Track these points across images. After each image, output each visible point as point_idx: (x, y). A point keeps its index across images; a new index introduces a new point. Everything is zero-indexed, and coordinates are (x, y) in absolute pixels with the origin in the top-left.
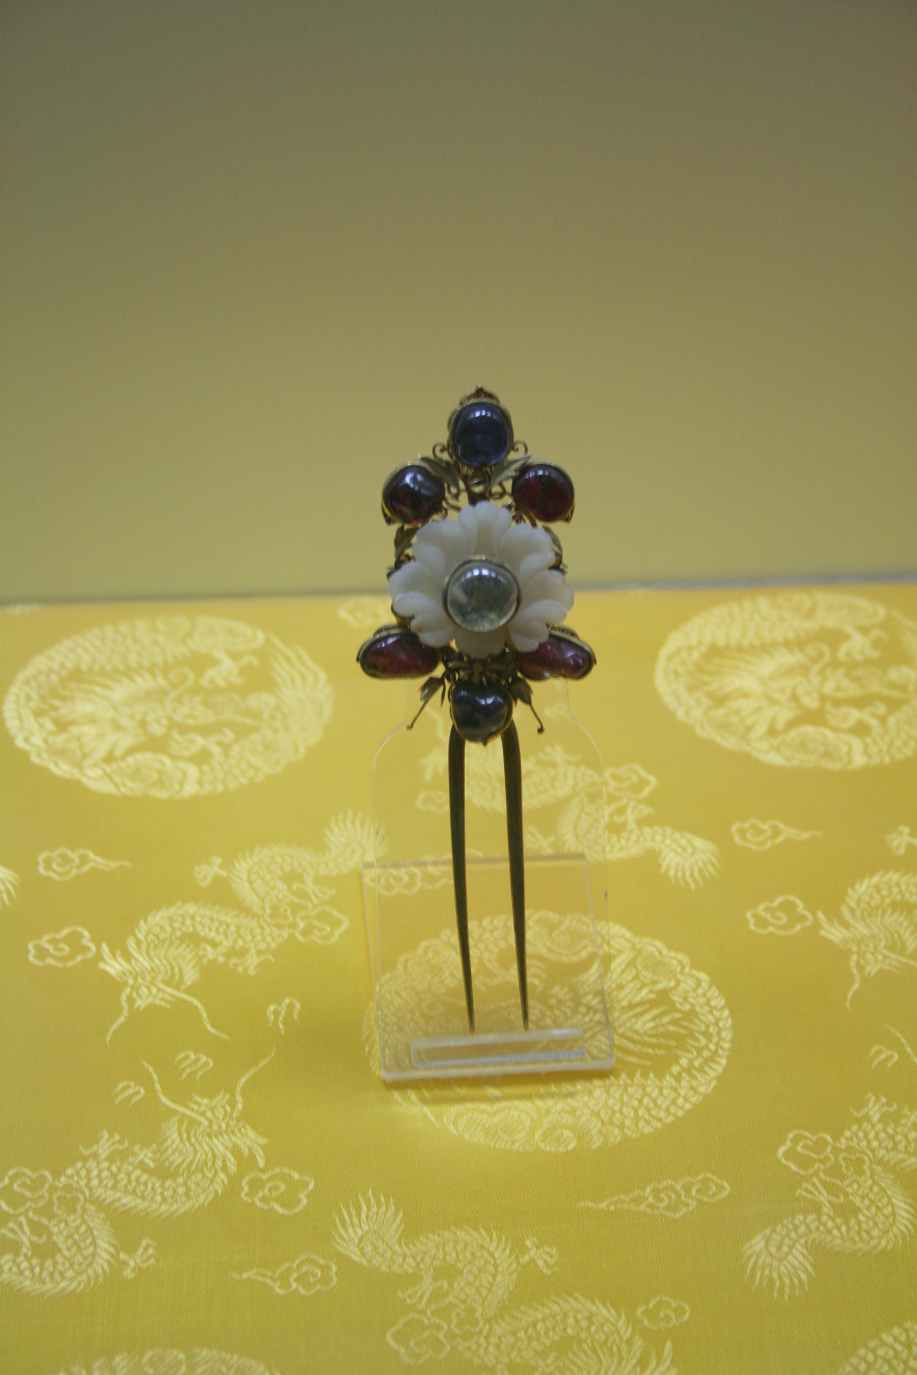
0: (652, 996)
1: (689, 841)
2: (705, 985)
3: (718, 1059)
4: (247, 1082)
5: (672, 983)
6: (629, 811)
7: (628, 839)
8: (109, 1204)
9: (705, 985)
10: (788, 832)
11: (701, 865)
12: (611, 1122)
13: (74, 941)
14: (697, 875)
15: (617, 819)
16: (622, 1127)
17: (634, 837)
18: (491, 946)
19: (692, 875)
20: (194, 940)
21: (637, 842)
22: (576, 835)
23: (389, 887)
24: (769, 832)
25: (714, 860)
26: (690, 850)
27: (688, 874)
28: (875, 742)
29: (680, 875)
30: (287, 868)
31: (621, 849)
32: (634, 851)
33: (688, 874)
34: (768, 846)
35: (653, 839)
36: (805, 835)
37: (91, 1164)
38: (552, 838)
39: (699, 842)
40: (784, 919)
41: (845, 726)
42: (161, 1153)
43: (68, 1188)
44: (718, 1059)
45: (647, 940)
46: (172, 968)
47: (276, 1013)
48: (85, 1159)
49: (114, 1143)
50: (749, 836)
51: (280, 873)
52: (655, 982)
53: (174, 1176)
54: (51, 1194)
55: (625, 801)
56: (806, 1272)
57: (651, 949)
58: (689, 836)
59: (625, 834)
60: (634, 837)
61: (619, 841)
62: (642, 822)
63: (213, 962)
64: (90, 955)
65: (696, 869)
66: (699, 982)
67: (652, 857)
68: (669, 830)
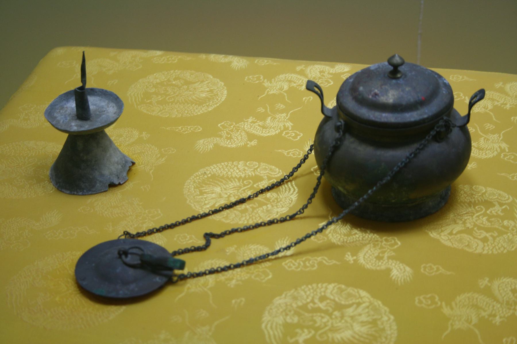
0: (205, 194)
1: (404, 267)
2: (391, 320)
3: (196, 176)
4: (292, 112)
5: (380, 317)
6: (386, 253)
7: (382, 263)
8: (247, 132)
9: (391, 320)
10: (442, 270)
11: (405, 277)
12: (235, 166)
13: (258, 79)
14: (402, 280)
15: (381, 255)
16: (232, 164)
17: (384, 262)
18: (490, 244)
19: (401, 280)
20: (476, 307)
21: (385, 265)
22: (364, 258)
23: (290, 267)
24: (435, 269)
25: (411, 276)
26: (403, 270)
27: (399, 279)
28: (488, 245)
29: (396, 279)
30: (321, 70)
31: (378, 266)
32: (383, 267)
33: (399, 279)
34: (433, 274)
35: (391, 265)
36: (449, 273)
37: (246, 123)
38: (355, 258)
39: (408, 269)
40: (429, 302)
41: (480, 237)
42: (265, 124)
43: (239, 127)
44: (196, 176)
45: (435, 237)
46: (282, 87)
47: (305, 99)
48: (244, 122)
49: (253, 120)
50: (427, 270)
51: (319, 70)
52: (373, 315)
53: (266, 128)
54: (233, 128)
55: (386, 249)
56: (410, 278)
57: (376, 303)
58: (404, 265)
59: (382, 261)
60: (384, 262)
61: (378, 263)
62: (389, 258)
63: (293, 87)
64: (261, 81)
65: (403, 278)
66: (389, 319)
67: (389, 271)
68: (398, 262)
